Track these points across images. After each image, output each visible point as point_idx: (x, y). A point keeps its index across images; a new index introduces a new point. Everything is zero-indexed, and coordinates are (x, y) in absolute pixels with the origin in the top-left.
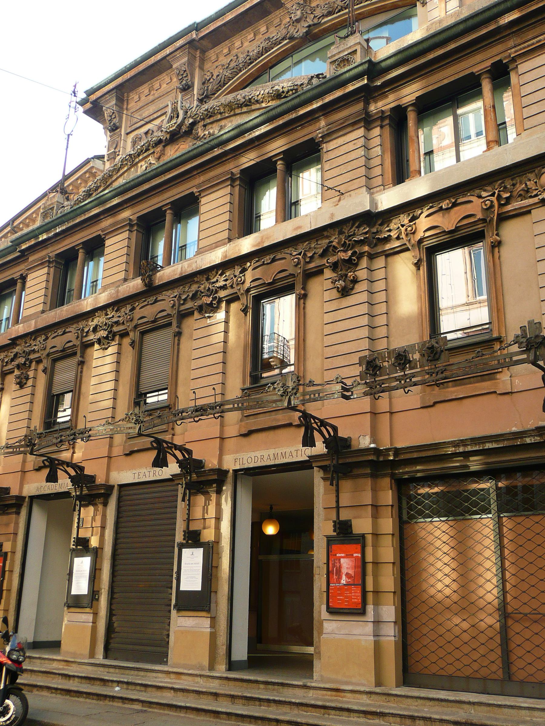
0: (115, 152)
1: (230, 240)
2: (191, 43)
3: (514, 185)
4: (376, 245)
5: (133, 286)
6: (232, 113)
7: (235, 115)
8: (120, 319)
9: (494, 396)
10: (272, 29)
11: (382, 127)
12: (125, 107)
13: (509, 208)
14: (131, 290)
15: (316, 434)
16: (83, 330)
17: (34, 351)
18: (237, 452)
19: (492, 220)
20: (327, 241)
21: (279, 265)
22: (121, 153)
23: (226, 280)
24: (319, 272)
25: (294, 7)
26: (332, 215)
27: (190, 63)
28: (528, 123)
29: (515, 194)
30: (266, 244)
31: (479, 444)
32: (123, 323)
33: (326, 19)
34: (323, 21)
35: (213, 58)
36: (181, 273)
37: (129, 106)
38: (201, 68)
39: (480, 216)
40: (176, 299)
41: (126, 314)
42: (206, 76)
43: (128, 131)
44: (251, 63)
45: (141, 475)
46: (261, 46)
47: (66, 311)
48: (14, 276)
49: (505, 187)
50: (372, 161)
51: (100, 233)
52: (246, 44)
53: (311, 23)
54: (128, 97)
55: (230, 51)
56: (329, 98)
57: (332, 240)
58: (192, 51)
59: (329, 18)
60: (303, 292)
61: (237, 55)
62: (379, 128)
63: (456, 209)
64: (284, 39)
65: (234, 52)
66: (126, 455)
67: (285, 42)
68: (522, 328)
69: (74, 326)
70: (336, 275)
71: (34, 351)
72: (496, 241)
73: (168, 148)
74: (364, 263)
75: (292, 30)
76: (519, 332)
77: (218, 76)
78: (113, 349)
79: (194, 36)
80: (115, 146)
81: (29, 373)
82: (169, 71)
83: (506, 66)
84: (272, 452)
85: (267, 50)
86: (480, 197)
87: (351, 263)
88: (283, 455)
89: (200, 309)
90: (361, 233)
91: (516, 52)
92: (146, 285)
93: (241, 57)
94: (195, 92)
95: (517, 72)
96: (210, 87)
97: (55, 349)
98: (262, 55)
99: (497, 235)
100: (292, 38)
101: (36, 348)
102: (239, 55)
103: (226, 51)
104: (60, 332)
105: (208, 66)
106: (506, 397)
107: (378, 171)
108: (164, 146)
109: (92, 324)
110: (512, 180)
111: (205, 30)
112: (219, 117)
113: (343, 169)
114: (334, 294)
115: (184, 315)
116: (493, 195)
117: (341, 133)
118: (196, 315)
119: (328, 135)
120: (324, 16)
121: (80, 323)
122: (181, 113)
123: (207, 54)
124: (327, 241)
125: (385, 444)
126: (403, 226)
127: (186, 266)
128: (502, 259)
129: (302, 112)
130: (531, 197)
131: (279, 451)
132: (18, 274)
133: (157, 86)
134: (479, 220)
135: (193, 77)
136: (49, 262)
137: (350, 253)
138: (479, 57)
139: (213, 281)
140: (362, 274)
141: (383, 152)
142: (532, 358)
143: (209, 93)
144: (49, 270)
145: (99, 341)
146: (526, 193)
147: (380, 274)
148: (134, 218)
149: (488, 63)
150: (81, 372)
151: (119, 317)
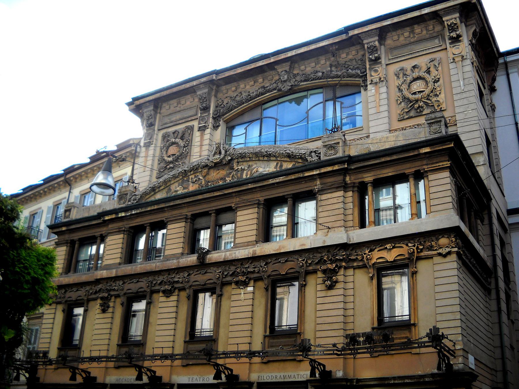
0: (150, 142)
1: (257, 242)
2: (212, 82)
3: (425, 242)
4: (348, 262)
5: (190, 261)
6: (257, 159)
7: (259, 160)
8: (180, 280)
9: (409, 354)
10: (266, 81)
11: (353, 191)
12: (159, 111)
13: (422, 254)
14: (189, 263)
15: (316, 370)
16: (152, 282)
17: (114, 290)
18: (260, 372)
19: (413, 259)
20: (320, 255)
21: (290, 264)
22: (154, 143)
23: (255, 268)
24: (315, 272)
25: (283, 73)
26: (324, 241)
27: (209, 93)
28: (433, 209)
29: (425, 247)
30: (282, 251)
31: (402, 380)
32: (182, 283)
33: (303, 83)
34: (301, 84)
35: (225, 91)
36: (224, 259)
37: (162, 111)
38: (216, 96)
39: (407, 256)
40: (220, 274)
41: (184, 277)
42: (218, 102)
43: (160, 128)
44: (251, 100)
45: (194, 380)
46: (259, 91)
47: (140, 268)
48: (96, 234)
49: (420, 242)
50: (347, 211)
51: (164, 219)
52: (248, 87)
53: (293, 84)
54: (162, 105)
55: (236, 89)
56: (323, 170)
57: (323, 255)
58: (211, 86)
59: (305, 83)
60: (304, 283)
61: (241, 93)
62: (351, 192)
63: (395, 249)
64: (275, 89)
65: (239, 90)
66: (183, 366)
67: (275, 91)
68: (430, 330)
69: (145, 278)
70: (324, 276)
71: (114, 290)
72: (415, 271)
73: (212, 171)
74: (342, 272)
75: (280, 85)
76: (429, 332)
77: (227, 103)
78: (174, 298)
79: (214, 78)
80: (149, 137)
81: (110, 303)
82: (193, 94)
83: (423, 174)
84: (282, 374)
85: (262, 94)
86: (407, 245)
87: (334, 272)
88: (290, 377)
89: (237, 283)
90: (341, 255)
91: (428, 168)
92: (200, 262)
93: (244, 95)
94: (211, 112)
95: (428, 179)
96: (221, 111)
97: (130, 291)
98: (259, 96)
99: (415, 267)
100: (280, 90)
101: (116, 288)
102: (242, 93)
103: (234, 89)
104: (134, 280)
105: (220, 95)
106: (416, 356)
107: (350, 217)
108: (209, 169)
109: (161, 278)
110: (424, 238)
111: (222, 75)
112: (248, 159)
113: (330, 213)
114: (323, 287)
115: (224, 284)
116: (414, 246)
117: (329, 191)
118: (233, 286)
119: (322, 190)
120: (301, 81)
121: (150, 277)
122: (223, 152)
123: (220, 88)
124: (320, 255)
125: (351, 376)
126: (365, 254)
127: (228, 255)
128: (417, 281)
129: (307, 174)
130: (433, 250)
131: (287, 374)
132: (99, 234)
133: (183, 102)
134: (406, 258)
135: (210, 102)
136: (124, 231)
137: (334, 265)
138: (408, 165)
139: (246, 266)
140: (341, 278)
141: (354, 207)
142: (434, 345)
143: (221, 114)
144: (124, 236)
145: (164, 292)
146: (431, 248)
147: (350, 279)
148: (189, 214)
149: (413, 170)
150: (150, 309)
151: (179, 278)
